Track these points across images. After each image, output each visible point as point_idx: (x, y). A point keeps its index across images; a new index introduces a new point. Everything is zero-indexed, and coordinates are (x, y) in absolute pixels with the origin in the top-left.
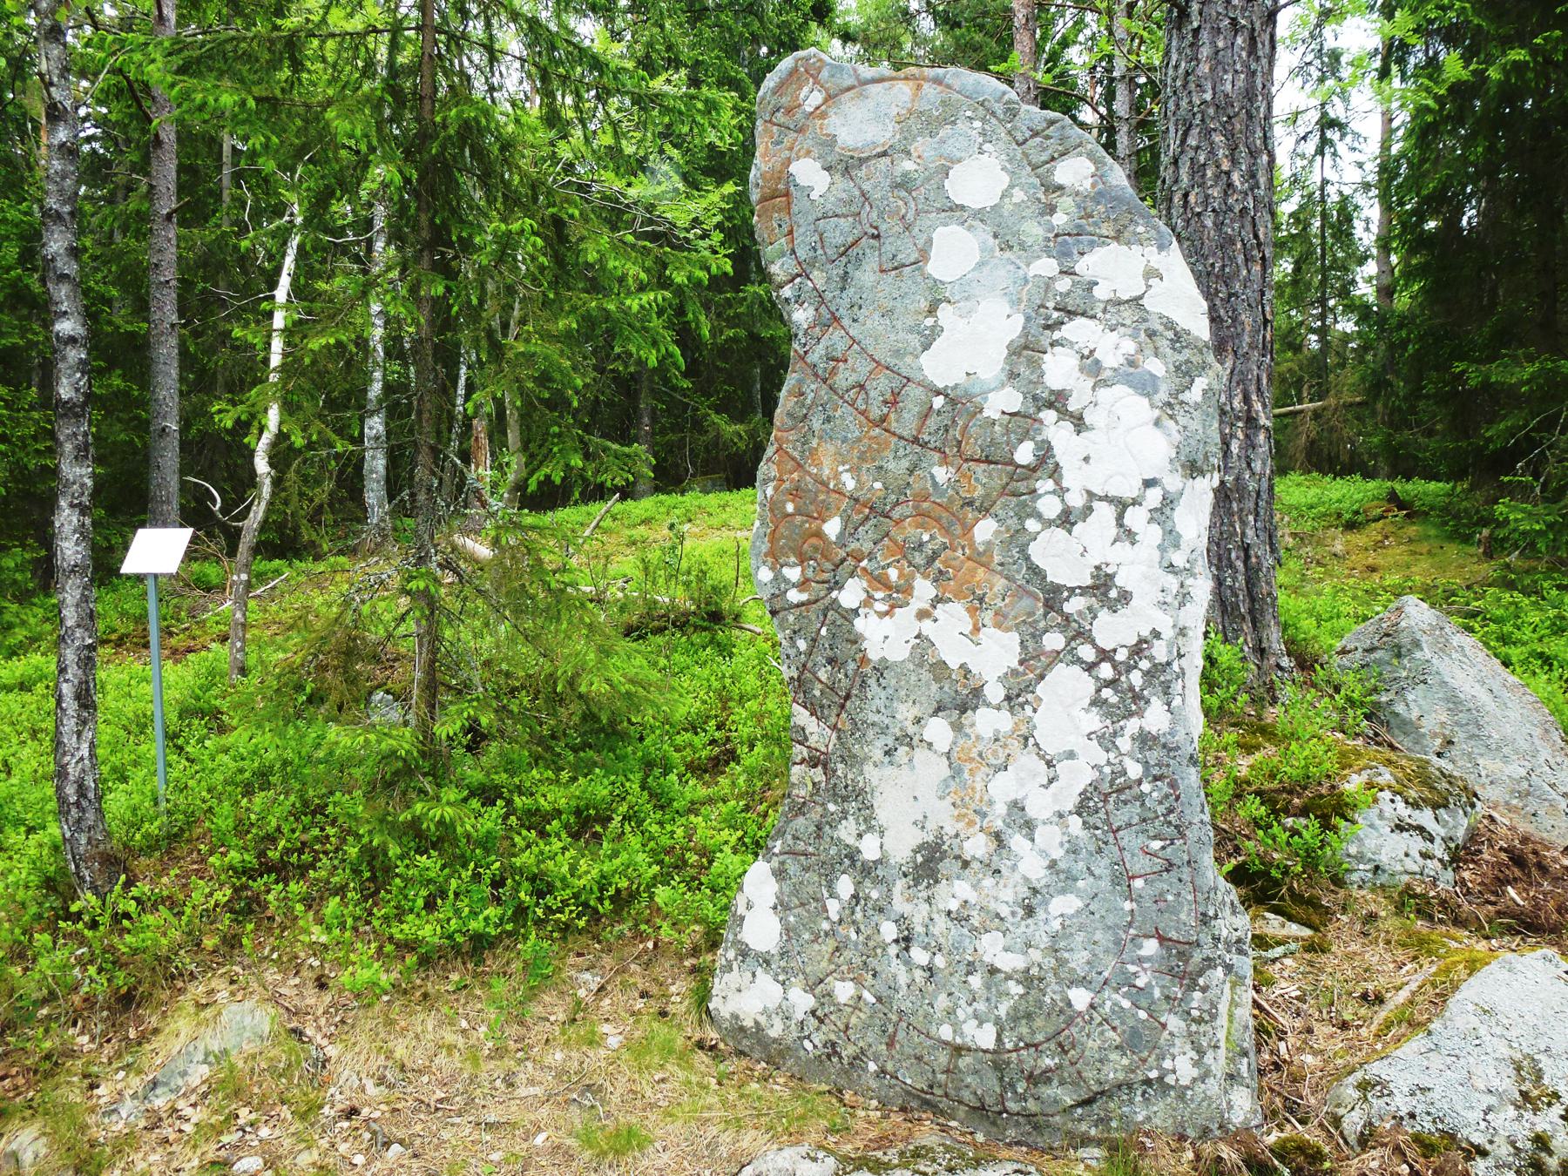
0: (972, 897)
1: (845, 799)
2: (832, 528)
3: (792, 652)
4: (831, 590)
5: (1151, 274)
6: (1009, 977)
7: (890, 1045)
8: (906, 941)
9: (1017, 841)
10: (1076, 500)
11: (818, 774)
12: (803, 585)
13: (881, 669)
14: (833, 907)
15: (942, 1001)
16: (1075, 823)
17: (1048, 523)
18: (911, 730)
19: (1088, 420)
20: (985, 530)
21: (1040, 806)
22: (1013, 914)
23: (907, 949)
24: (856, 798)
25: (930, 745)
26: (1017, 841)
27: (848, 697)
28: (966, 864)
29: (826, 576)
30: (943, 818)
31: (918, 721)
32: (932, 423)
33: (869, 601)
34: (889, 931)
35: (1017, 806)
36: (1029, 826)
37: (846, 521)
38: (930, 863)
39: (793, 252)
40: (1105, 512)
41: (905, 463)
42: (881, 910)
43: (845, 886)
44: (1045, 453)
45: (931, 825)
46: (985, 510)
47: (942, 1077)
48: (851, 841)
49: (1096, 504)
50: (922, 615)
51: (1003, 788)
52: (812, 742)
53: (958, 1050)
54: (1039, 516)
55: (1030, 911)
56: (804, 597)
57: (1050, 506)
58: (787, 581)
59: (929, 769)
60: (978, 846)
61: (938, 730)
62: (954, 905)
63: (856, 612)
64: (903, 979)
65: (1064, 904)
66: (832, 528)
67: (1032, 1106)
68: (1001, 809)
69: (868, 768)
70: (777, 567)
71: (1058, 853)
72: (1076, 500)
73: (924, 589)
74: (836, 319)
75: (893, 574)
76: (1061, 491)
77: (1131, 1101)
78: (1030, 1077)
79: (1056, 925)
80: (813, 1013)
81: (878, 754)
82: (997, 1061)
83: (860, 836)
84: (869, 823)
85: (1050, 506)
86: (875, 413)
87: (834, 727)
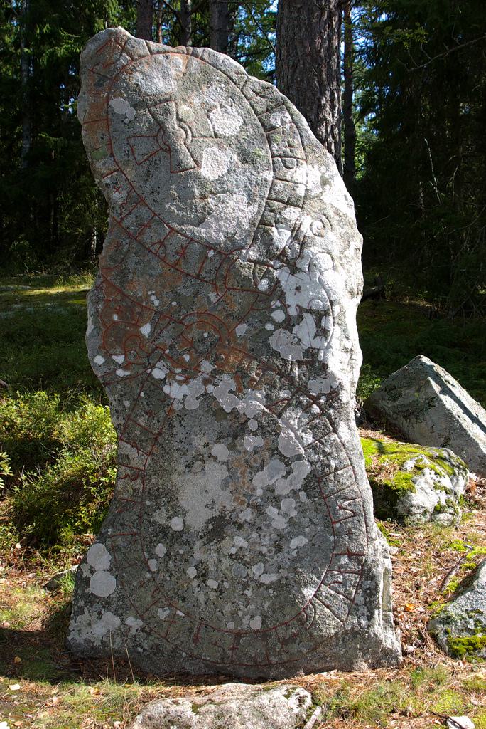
0: (245, 545)
1: (157, 497)
2: (146, 330)
3: (120, 409)
4: (145, 368)
5: (325, 182)
6: (268, 587)
7: (196, 640)
8: (203, 575)
9: (271, 511)
10: (293, 312)
11: (138, 484)
12: (125, 366)
13: (182, 415)
14: (153, 563)
15: (228, 607)
16: (303, 495)
17: (278, 326)
18: (203, 450)
19: (298, 266)
20: (241, 330)
21: (283, 488)
22: (269, 551)
23: (204, 582)
24: (168, 497)
25: (215, 458)
26: (271, 511)
27: (160, 434)
28: (240, 526)
29: (145, 360)
30: (226, 501)
31: (207, 445)
32: (207, 265)
33: (172, 374)
34: (192, 572)
35: (270, 489)
36: (277, 501)
37: (155, 326)
38: (218, 528)
39: (112, 155)
40: (309, 319)
41: (192, 290)
42: (187, 561)
43: (161, 549)
44: (275, 284)
45: (218, 506)
46: (242, 320)
47: (230, 653)
48: (163, 522)
49: (305, 315)
50: (206, 382)
51: (261, 480)
52: (134, 464)
53: (238, 635)
54: (272, 321)
55: (279, 549)
56: (128, 373)
57: (279, 316)
58: (116, 364)
59: (216, 473)
60: (247, 515)
61: (220, 450)
62: (233, 551)
63: (163, 381)
64: (202, 599)
65: (298, 542)
66: (146, 330)
67: (285, 657)
68: (259, 492)
69: (175, 477)
70: (108, 357)
71: (294, 514)
72: (293, 312)
73: (207, 367)
74: (142, 201)
75: (187, 357)
76: (285, 307)
77: (337, 645)
78: (285, 642)
79: (294, 554)
80: (143, 629)
81: (181, 467)
82: (263, 634)
83: (169, 518)
84: (176, 511)
85: (279, 316)
86: (171, 259)
87: (151, 454)
